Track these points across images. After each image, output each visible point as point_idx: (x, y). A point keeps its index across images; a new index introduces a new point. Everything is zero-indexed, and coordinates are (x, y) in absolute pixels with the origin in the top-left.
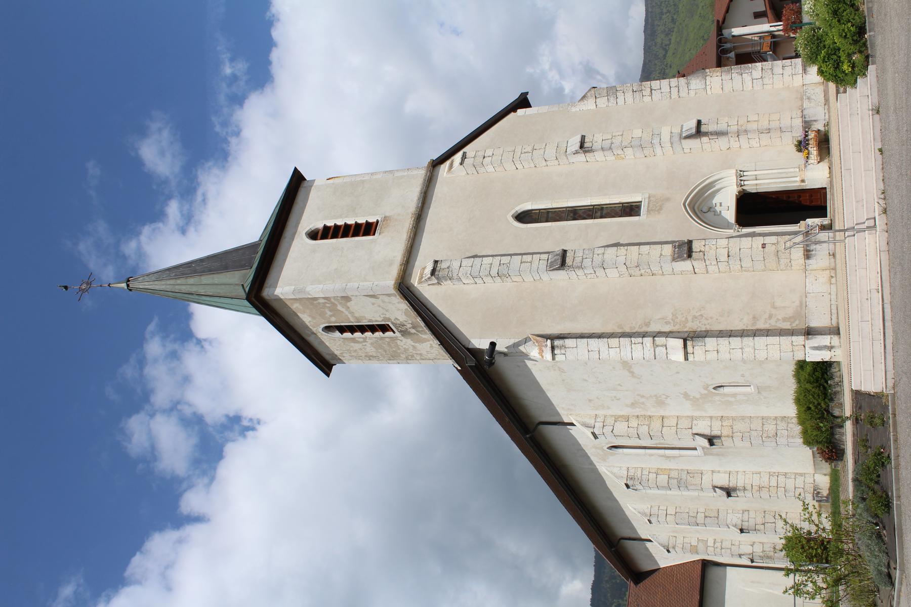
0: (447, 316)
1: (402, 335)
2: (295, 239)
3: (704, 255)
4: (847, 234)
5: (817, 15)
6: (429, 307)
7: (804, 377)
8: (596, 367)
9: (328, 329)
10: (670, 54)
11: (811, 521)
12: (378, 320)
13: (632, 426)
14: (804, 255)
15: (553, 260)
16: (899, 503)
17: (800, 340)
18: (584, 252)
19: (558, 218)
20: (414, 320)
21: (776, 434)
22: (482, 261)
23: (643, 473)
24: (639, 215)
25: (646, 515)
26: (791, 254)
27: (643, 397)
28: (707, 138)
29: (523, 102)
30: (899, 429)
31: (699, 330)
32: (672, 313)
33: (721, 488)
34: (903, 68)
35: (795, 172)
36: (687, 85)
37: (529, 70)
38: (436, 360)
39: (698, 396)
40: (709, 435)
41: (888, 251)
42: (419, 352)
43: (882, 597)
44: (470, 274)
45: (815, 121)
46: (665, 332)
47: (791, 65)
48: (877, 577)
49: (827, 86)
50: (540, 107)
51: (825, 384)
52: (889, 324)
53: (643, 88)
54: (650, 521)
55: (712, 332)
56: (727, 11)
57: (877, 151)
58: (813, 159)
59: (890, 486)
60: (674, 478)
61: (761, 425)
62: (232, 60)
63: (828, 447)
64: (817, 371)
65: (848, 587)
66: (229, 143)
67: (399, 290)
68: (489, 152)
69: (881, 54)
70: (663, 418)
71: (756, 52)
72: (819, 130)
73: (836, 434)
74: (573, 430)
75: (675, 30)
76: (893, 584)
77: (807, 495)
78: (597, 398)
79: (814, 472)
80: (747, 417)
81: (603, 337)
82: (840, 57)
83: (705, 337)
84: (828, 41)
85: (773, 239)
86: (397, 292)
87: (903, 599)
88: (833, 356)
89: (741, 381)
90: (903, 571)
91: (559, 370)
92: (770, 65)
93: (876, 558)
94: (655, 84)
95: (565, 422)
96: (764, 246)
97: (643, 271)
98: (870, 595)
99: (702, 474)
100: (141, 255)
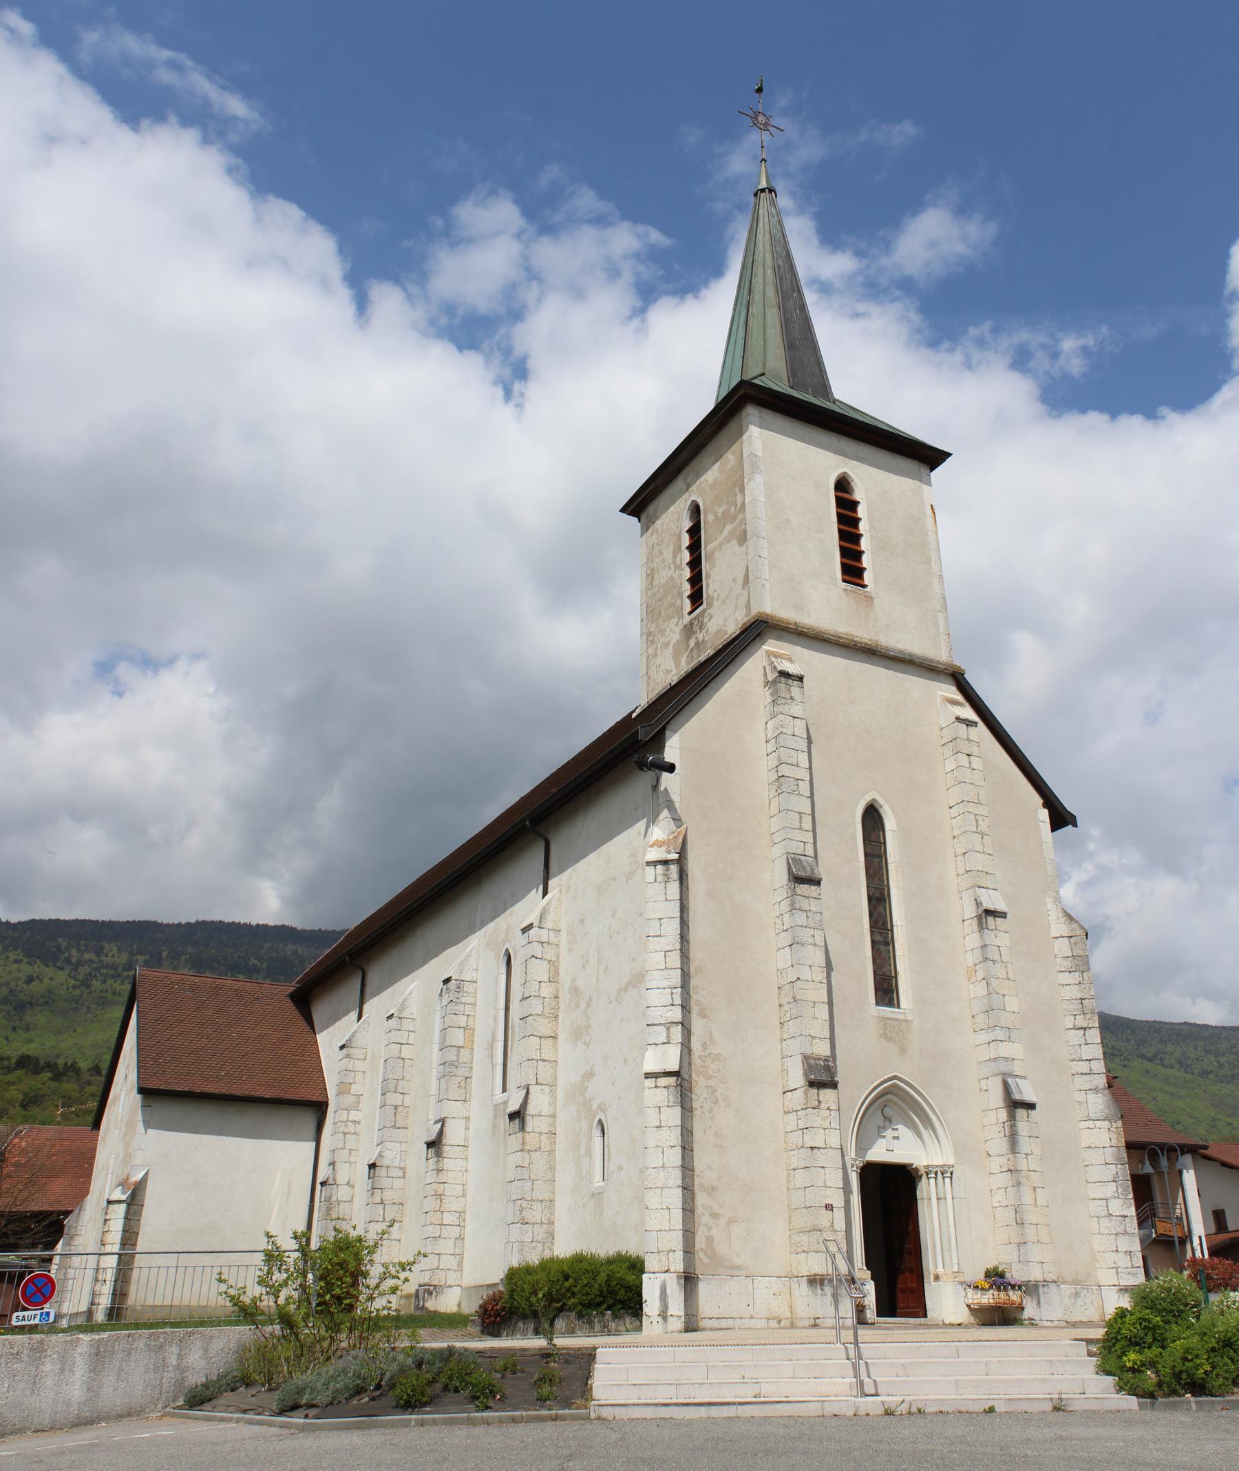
0: (716, 697)
3: (814, 1108)
5: (1222, 1313)
7: (618, 1269)
9: (695, 510)
11: (383, 1278)
12: (710, 587)
14: (815, 1275)
16: (413, 1423)
17: (678, 1265)
18: (816, 913)
19: (871, 872)
20: (709, 645)
21: (527, 1223)
24: (877, 1004)
25: (400, 1011)
26: (816, 1252)
27: (588, 1006)
28: (1006, 1119)
29: (1060, 818)
30: (532, 1426)
31: (694, 1097)
33: (441, 1132)
34: (1135, 1454)
35: (952, 1264)
36: (1093, 1088)
38: (646, 679)
39: (588, 1095)
41: (823, 1416)
42: (659, 652)
45: (1039, 1302)
46: (689, 1041)
47: (1133, 1267)
48: (293, 1387)
49: (1099, 1326)
50: (1052, 845)
51: (605, 1306)
52: (702, 1412)
53: (1088, 1016)
56: (1224, 1164)
58: (975, 1297)
59: (441, 1409)
60: (458, 1055)
61: (541, 1198)
63: (503, 1309)
64: (626, 1292)
67: (757, 620)
70: (554, 1037)
71: (1154, 1210)
72: (1023, 1309)
73: (524, 1324)
74: (536, 894)
75: (1189, 1077)
76: (281, 1413)
78: (586, 933)
80: (554, 1176)
81: (682, 943)
84: (1176, 1329)
85: (840, 1224)
87: (257, 1429)
88: (652, 1319)
89: (611, 1166)
90: (302, 1429)
93: (324, 1385)
94: (1095, 1035)
95: (550, 882)
96: (829, 1207)
97: (787, 1007)
98: (265, 1374)
99: (465, 1101)
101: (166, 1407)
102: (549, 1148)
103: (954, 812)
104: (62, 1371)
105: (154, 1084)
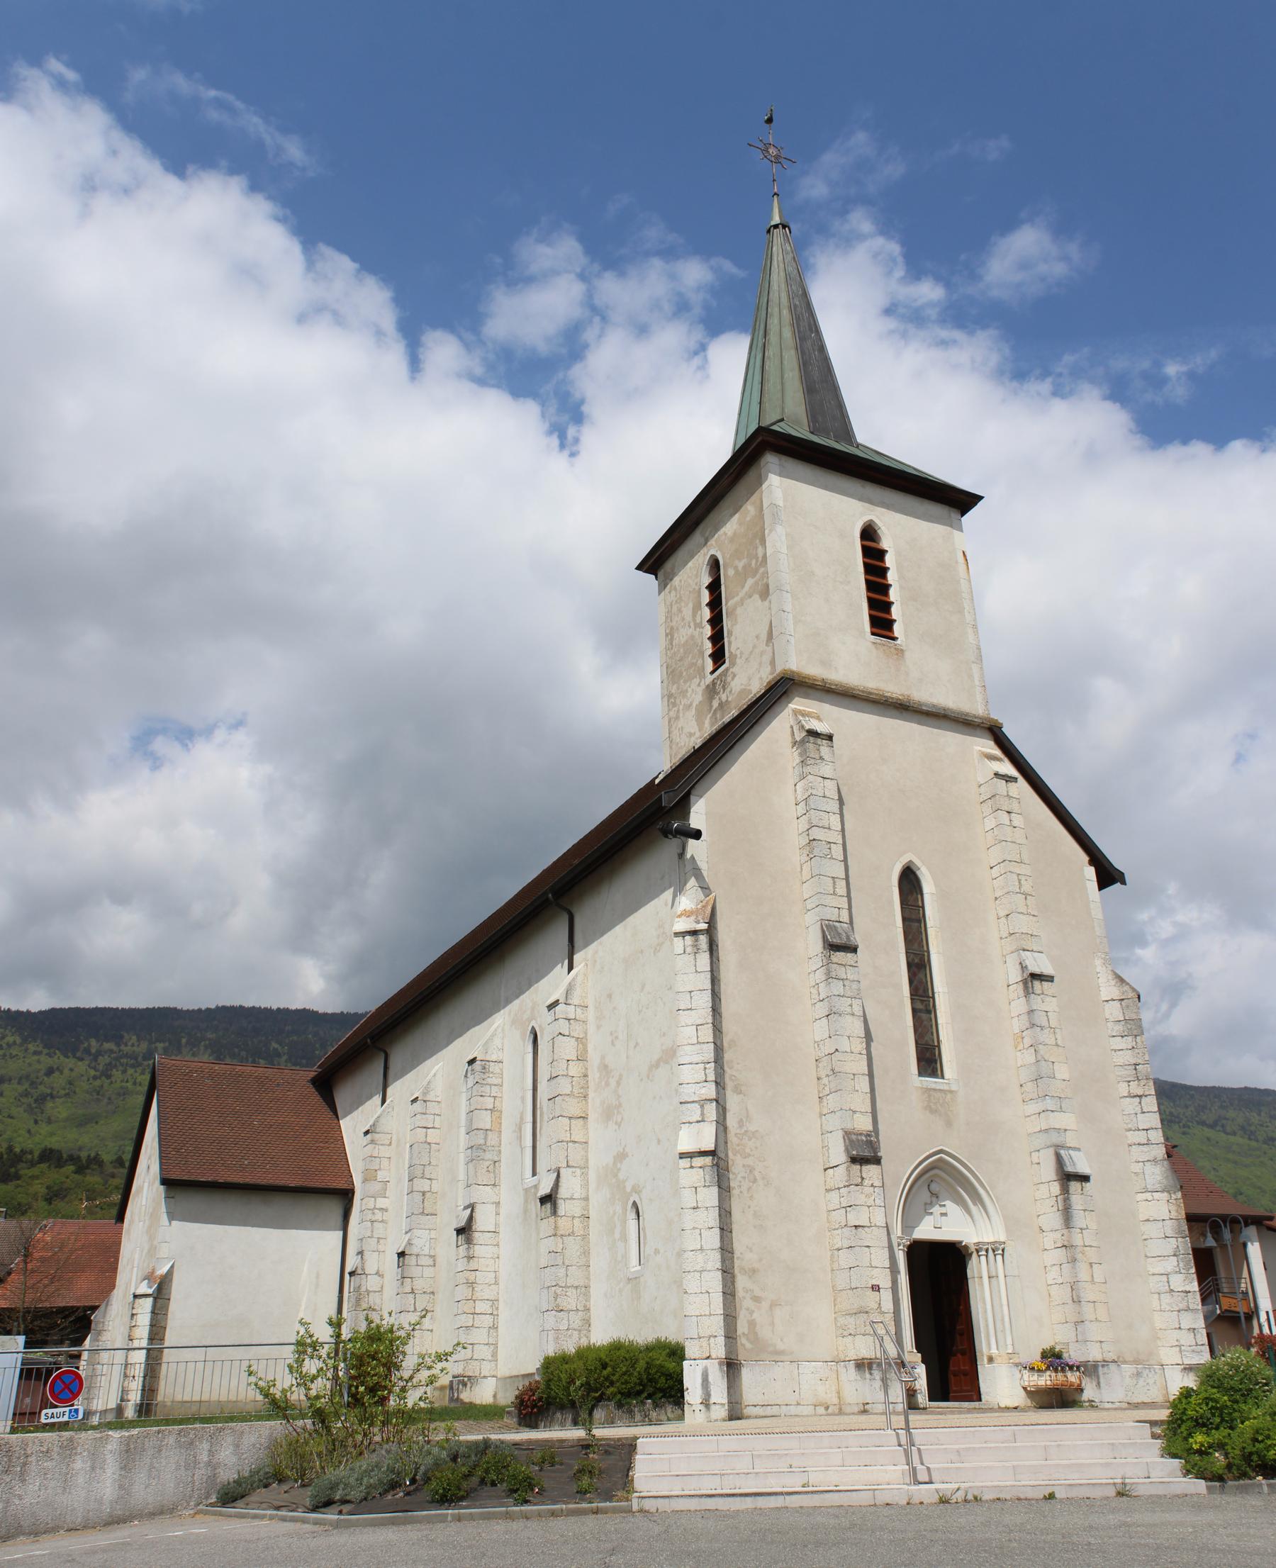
1: (708, 686)
2: (861, 503)
3: (857, 1185)
4: (902, 1432)
6: (757, 728)
8: (664, 1004)
9: (715, 565)
10: (1208, 1132)
12: (732, 645)
13: (570, 1067)
14: (863, 1359)
15: (840, 930)
16: (449, 1518)
17: (719, 1350)
19: (910, 937)
20: (733, 705)
22: (834, 813)
23: (493, 1087)
24: (920, 1074)
25: (425, 1094)
26: (864, 1335)
27: (618, 1083)
29: (1107, 876)
30: (573, 1519)
31: (731, 1176)
32: (757, 1131)
33: (471, 1218)
37: (1172, 888)
39: (621, 1176)
40: (558, 1196)
41: (875, 1505)
42: (681, 715)
43: (293, 1492)
44: (811, 794)
45: (1099, 1384)
46: (725, 1118)
49: (1162, 1407)
52: (749, 1503)
53: (1143, 1082)
54: (415, 1100)
55: (728, 1198)
57: (1050, 1490)
58: (1031, 1379)
59: (478, 1503)
60: (486, 1139)
62: (1191, 376)
63: (540, 1399)
64: (667, 1380)
65: (310, 1434)
66: (1043, 380)
67: (783, 678)
68: (1018, 821)
69: (1228, 1503)
71: (1217, 1285)
72: (1082, 1390)
73: (562, 1414)
74: (560, 969)
75: (1254, 1144)
76: (315, 1509)
77: (461, 1365)
78: (615, 1008)
79: (499, 1376)
81: (714, 1016)
82: (1217, 1428)
83: (719, 1187)
85: (888, 1305)
86: (778, 675)
87: (290, 1526)
88: (694, 1408)
89: (648, 1250)
90: (337, 1525)
91: (658, 945)
92: (1196, 1307)
93: (357, 1480)
94: (1151, 1103)
95: (575, 956)
96: (876, 1288)
97: (825, 1080)
98: (297, 1470)
99: (494, 1185)
100: (849, 241)
101: (198, 1505)
102: (582, 1232)
103: (995, 872)
104: (93, 1468)
105: (174, 1176)
